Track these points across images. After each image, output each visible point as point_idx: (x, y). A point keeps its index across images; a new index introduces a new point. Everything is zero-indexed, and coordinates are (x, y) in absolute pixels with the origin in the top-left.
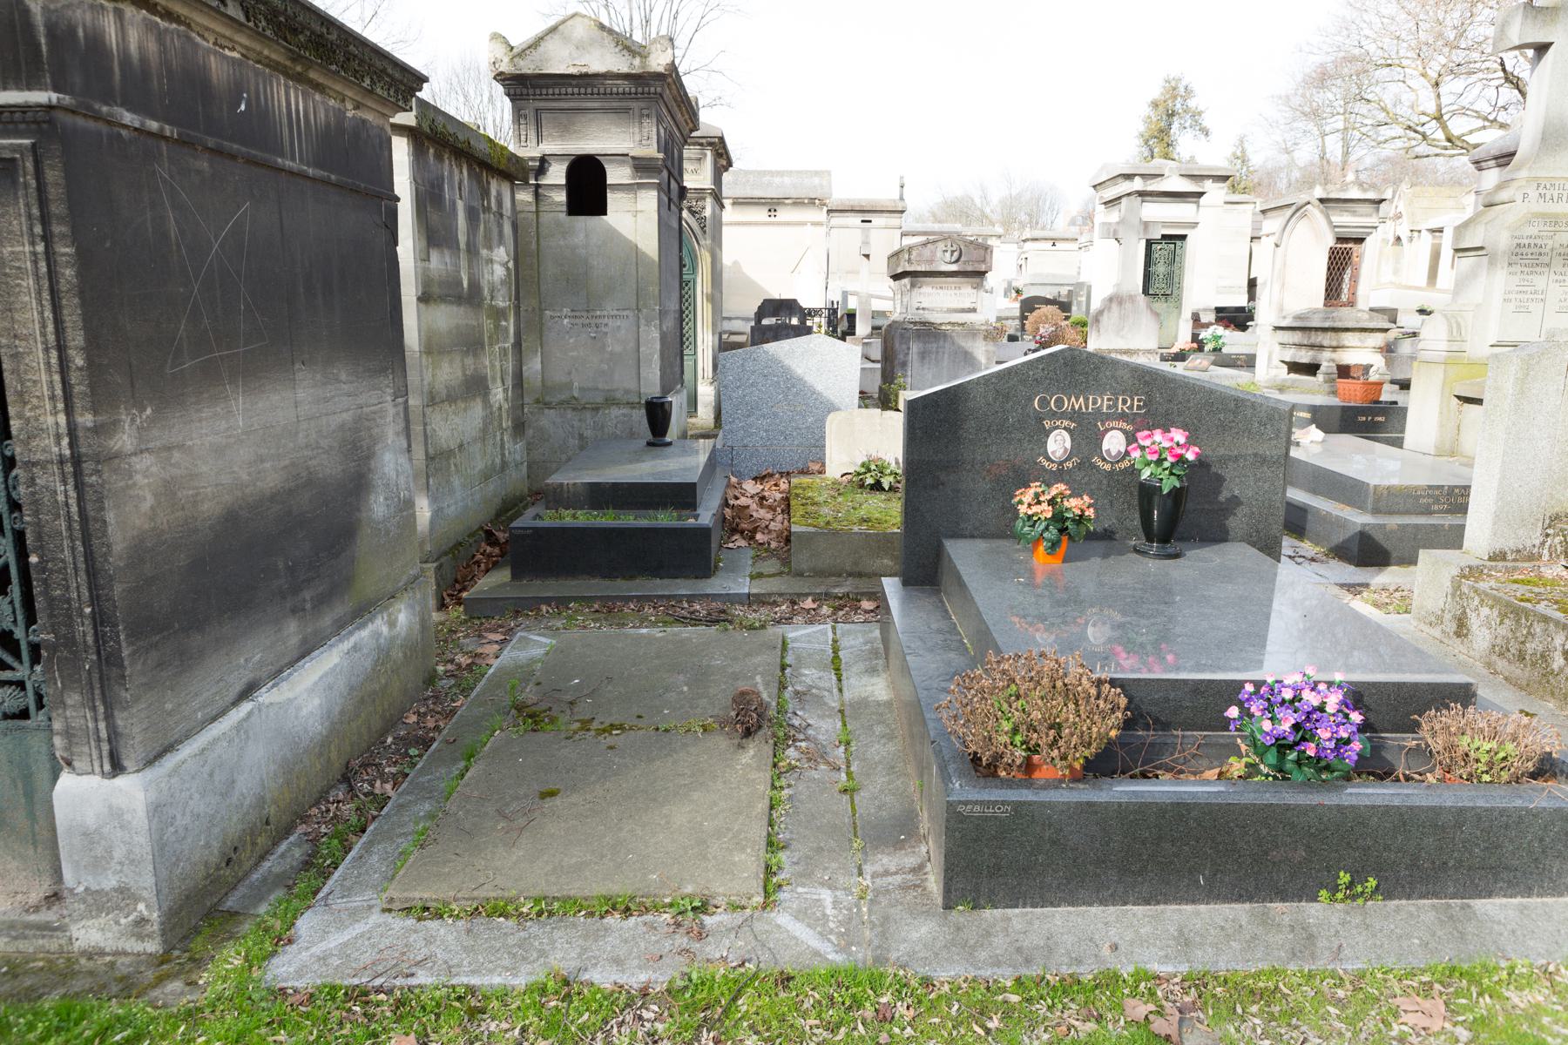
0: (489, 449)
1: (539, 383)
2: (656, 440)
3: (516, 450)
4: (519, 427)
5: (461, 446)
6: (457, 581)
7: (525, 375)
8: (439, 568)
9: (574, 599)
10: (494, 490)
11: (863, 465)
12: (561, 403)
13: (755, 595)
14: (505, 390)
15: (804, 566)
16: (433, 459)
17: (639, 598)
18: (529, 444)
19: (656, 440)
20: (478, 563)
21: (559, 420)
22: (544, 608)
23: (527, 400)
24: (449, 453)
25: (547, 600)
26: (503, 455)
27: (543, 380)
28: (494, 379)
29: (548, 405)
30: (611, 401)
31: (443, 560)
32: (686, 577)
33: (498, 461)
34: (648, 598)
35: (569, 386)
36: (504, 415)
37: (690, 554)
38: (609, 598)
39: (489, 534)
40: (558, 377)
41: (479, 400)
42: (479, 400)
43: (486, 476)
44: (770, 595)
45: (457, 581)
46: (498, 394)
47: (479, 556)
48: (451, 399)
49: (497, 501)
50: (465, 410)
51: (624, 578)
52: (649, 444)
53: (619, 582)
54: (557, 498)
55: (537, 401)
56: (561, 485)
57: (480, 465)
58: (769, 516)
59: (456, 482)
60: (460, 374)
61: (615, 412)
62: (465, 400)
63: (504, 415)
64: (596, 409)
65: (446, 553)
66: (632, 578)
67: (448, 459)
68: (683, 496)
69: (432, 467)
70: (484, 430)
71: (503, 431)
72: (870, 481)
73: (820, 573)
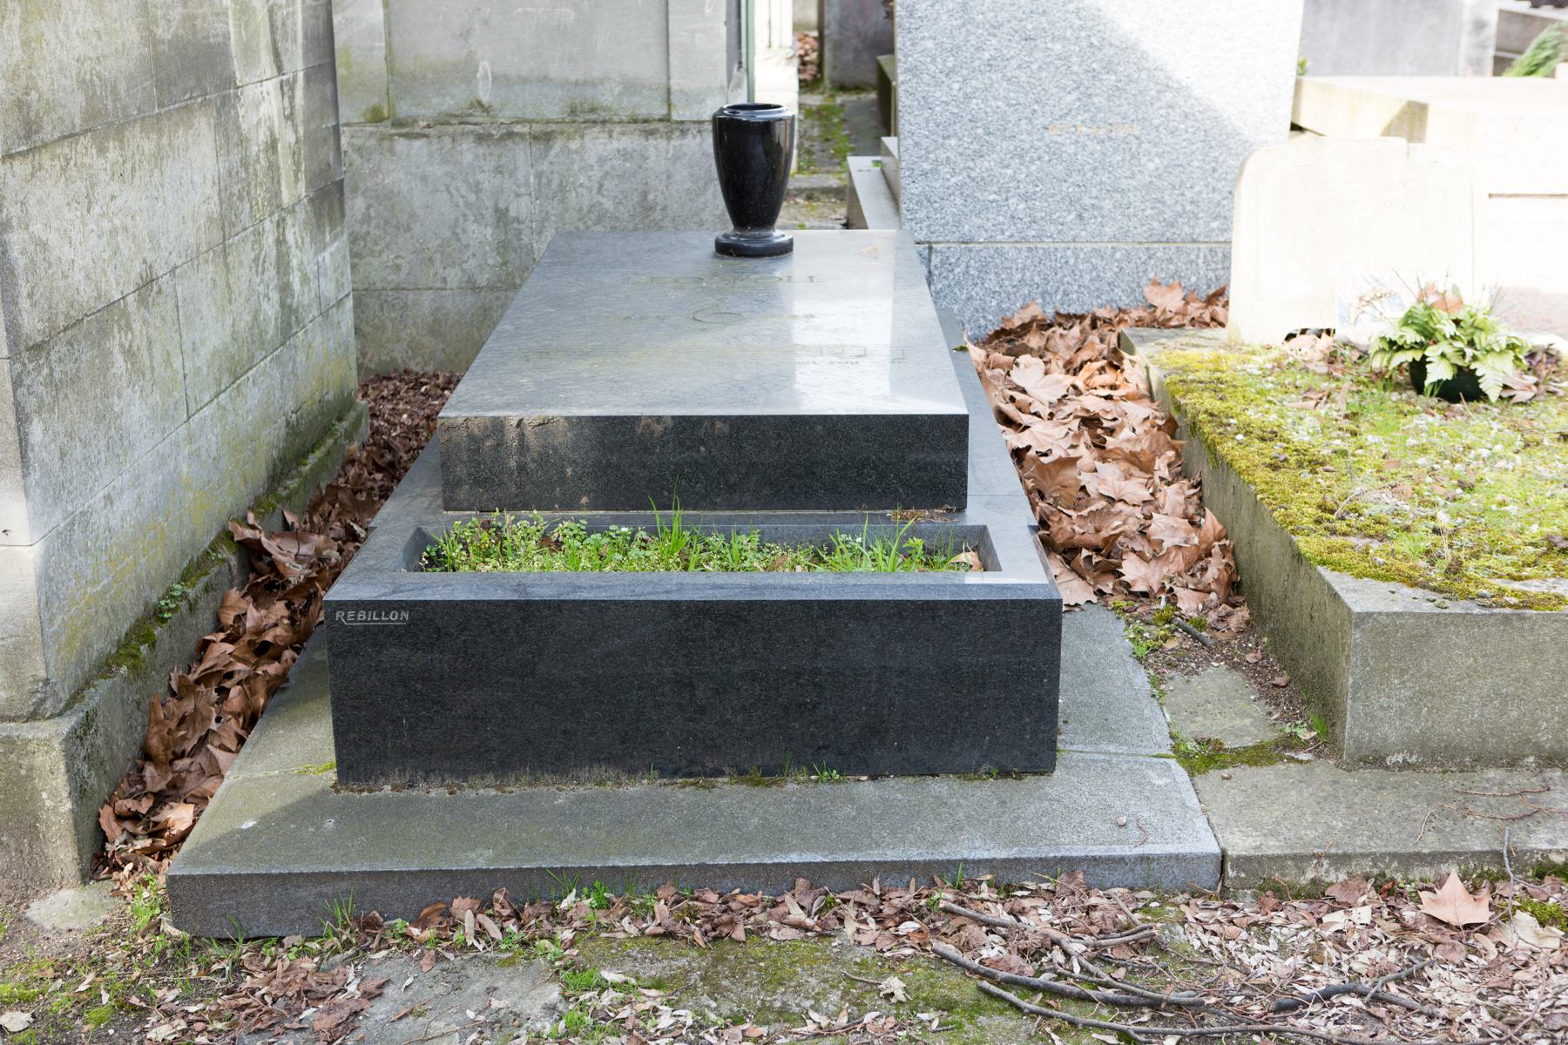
0: (243, 275)
1: (378, 65)
2: (745, 239)
3: (321, 267)
4: (329, 197)
5: (147, 283)
6: (147, 756)
7: (340, 39)
8: (78, 736)
9: (582, 879)
10: (263, 406)
11: (1409, 320)
12: (443, 121)
13: (1243, 862)
14: (286, 88)
15: (1391, 731)
16: (37, 348)
17: (816, 874)
18: (354, 239)
19: (745, 239)
20: (219, 679)
21: (437, 170)
22: (463, 908)
23: (346, 113)
24: (109, 314)
25: (480, 886)
26: (285, 289)
27: (390, 57)
28: (249, 52)
29: (404, 127)
30: (586, 116)
31: (95, 697)
32: (965, 771)
33: (271, 310)
34: (856, 874)
35: (465, 71)
36: (285, 163)
37: (977, 691)
38: (704, 874)
39: (252, 552)
40: (433, 44)
41: (203, 124)
42: (203, 124)
43: (235, 370)
44: (1300, 860)
45: (147, 756)
46: (266, 102)
47: (221, 650)
48: (102, 124)
49: (272, 436)
50: (158, 158)
51: (742, 773)
52: (725, 249)
53: (729, 794)
54: (499, 475)
55: (376, 117)
56: (498, 426)
57: (213, 334)
58: (1136, 489)
59: (134, 408)
60: (133, 36)
61: (597, 145)
62: (153, 124)
63: (285, 163)
64: (545, 138)
65: (105, 667)
66: (771, 773)
67: (104, 333)
68: (906, 464)
69: (37, 380)
70: (225, 223)
71: (281, 214)
72: (1439, 371)
73: (1440, 756)
